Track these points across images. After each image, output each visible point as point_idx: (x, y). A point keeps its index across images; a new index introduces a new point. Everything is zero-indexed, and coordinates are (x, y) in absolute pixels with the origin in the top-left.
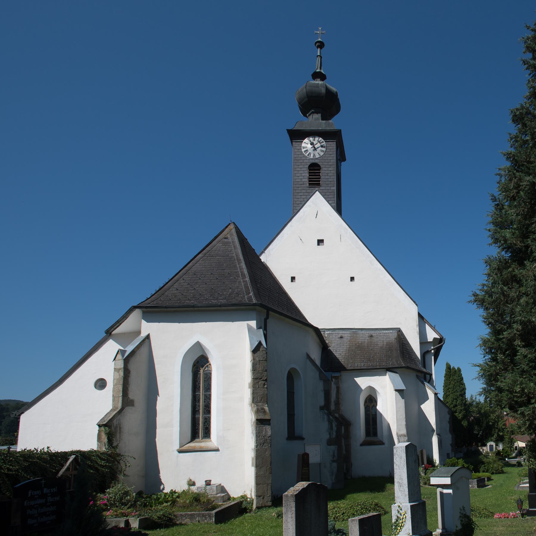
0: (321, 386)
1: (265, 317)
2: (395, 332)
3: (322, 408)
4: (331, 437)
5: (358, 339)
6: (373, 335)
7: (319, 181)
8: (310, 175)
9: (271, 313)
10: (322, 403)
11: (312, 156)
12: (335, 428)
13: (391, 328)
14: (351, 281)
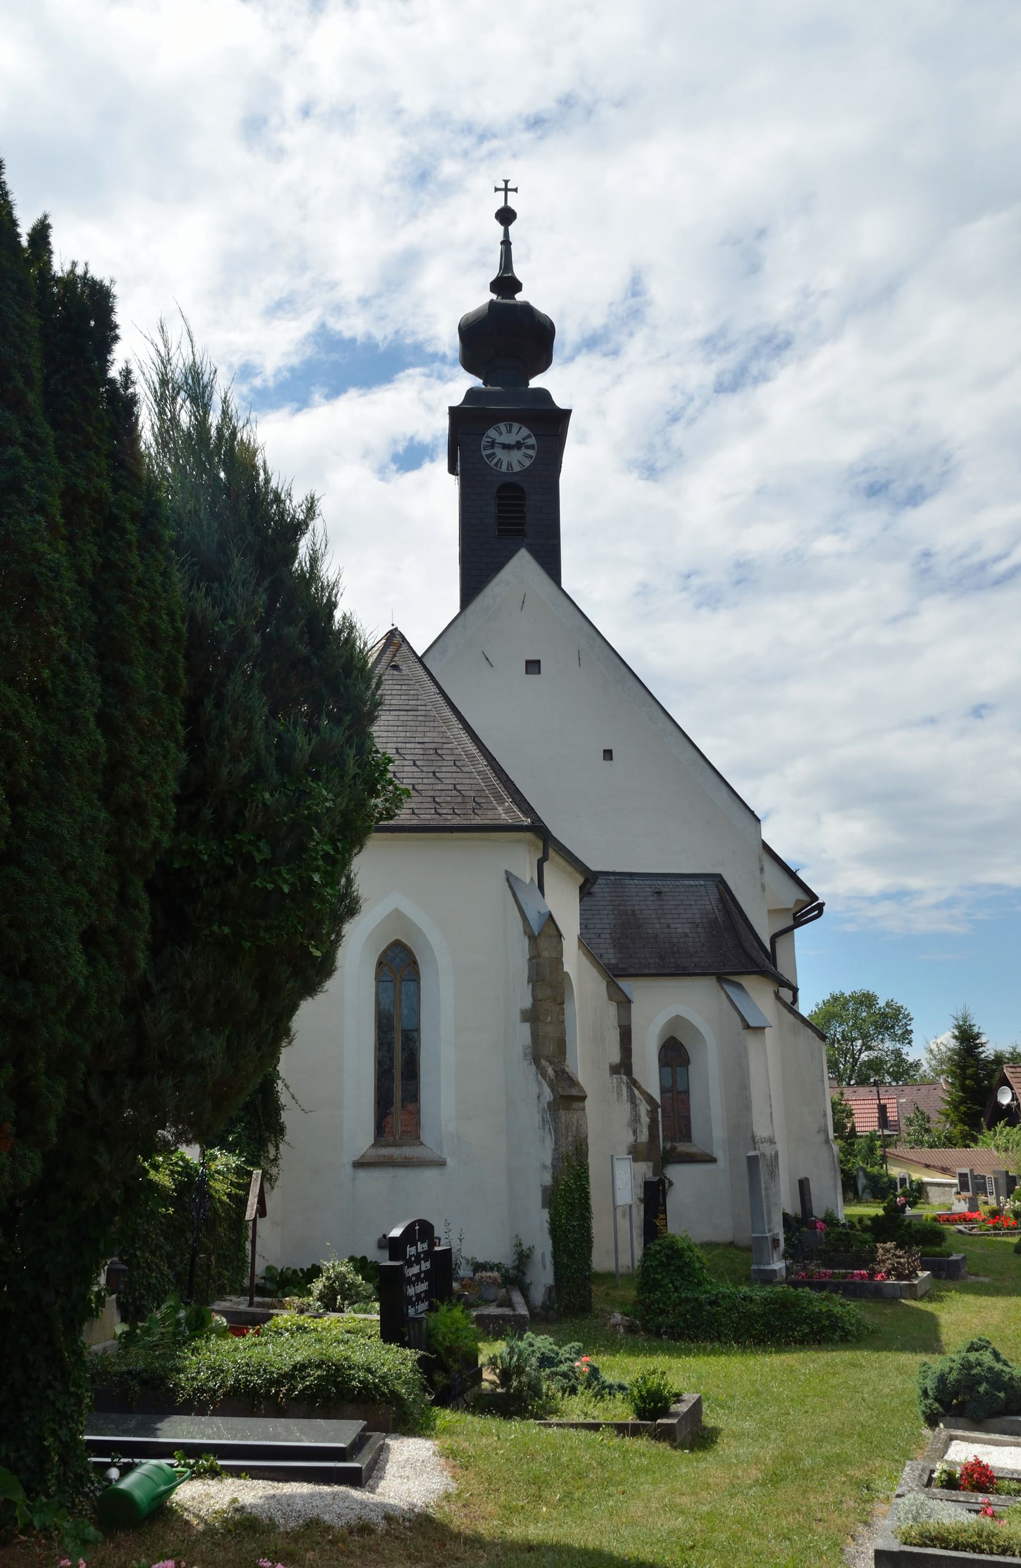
0: (611, 1011)
1: (541, 856)
2: (711, 883)
3: (615, 1070)
4: (639, 1141)
5: (630, 899)
6: (663, 890)
7: (522, 524)
8: (499, 511)
9: (552, 853)
10: (616, 1058)
11: (504, 469)
12: (645, 1120)
13: (700, 874)
14: (605, 751)
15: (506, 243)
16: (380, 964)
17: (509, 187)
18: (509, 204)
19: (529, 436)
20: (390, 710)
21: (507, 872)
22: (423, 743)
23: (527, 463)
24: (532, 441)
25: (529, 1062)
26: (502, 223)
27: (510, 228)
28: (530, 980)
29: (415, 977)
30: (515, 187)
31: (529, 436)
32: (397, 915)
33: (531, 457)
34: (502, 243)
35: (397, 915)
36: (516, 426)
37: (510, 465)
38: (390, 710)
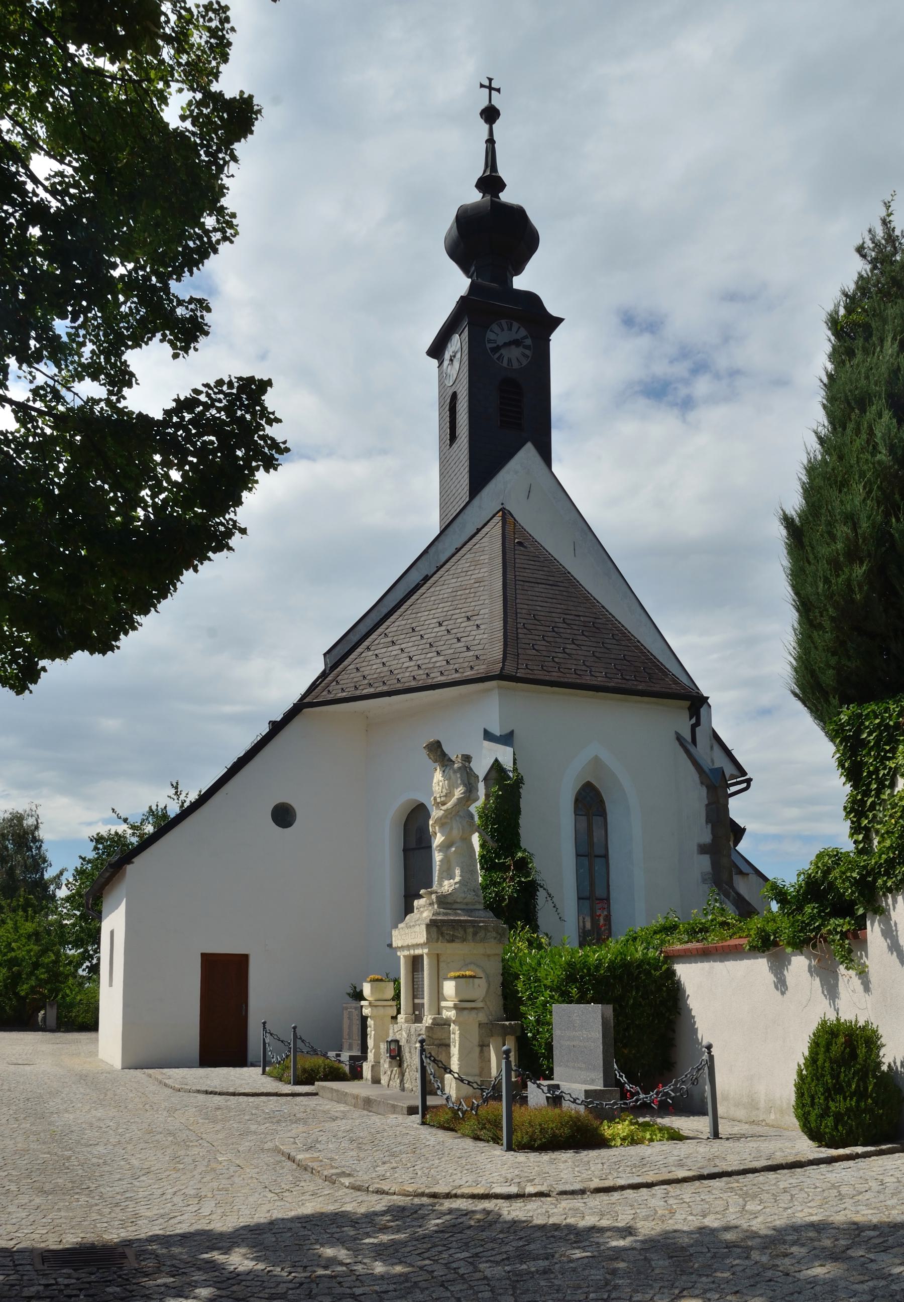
11: (505, 364)
15: (491, 141)
16: (577, 801)
17: (493, 86)
18: (493, 103)
19: (526, 337)
20: (538, 583)
21: (677, 733)
22: (579, 616)
23: (525, 362)
24: (528, 342)
25: (710, 885)
26: (486, 121)
27: (494, 126)
28: (709, 820)
29: (603, 813)
30: (498, 87)
31: (526, 337)
32: (596, 762)
33: (528, 357)
34: (487, 141)
35: (596, 762)
36: (516, 325)
37: (510, 360)
38: (538, 583)
